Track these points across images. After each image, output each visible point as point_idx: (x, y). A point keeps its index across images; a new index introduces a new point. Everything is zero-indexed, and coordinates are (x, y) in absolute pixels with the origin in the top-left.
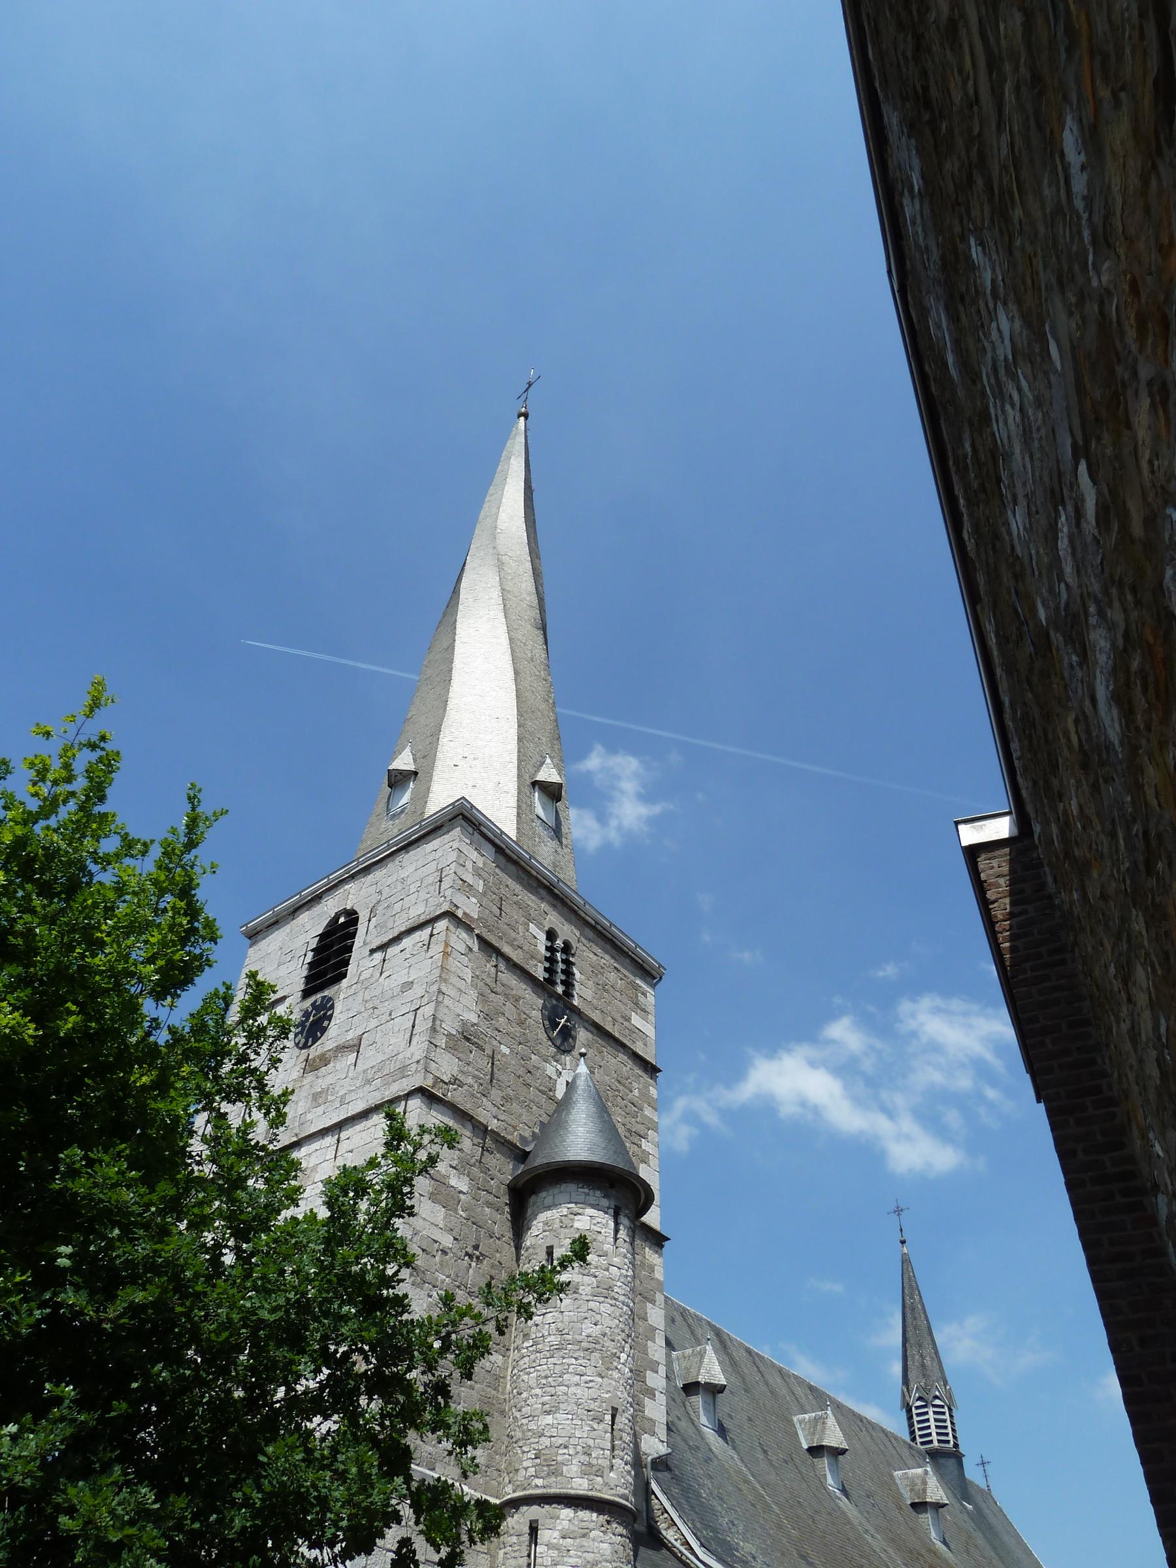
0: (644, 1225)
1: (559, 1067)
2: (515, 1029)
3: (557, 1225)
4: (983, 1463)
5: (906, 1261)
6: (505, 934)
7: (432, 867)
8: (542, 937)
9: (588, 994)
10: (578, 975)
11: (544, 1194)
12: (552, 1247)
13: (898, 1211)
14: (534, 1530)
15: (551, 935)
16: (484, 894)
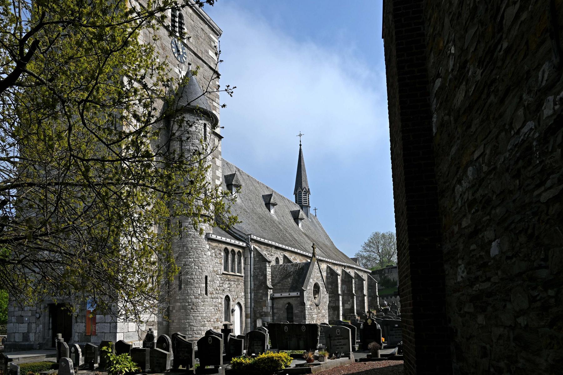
5: (300, 149)
10: (186, 30)
13: (300, 135)
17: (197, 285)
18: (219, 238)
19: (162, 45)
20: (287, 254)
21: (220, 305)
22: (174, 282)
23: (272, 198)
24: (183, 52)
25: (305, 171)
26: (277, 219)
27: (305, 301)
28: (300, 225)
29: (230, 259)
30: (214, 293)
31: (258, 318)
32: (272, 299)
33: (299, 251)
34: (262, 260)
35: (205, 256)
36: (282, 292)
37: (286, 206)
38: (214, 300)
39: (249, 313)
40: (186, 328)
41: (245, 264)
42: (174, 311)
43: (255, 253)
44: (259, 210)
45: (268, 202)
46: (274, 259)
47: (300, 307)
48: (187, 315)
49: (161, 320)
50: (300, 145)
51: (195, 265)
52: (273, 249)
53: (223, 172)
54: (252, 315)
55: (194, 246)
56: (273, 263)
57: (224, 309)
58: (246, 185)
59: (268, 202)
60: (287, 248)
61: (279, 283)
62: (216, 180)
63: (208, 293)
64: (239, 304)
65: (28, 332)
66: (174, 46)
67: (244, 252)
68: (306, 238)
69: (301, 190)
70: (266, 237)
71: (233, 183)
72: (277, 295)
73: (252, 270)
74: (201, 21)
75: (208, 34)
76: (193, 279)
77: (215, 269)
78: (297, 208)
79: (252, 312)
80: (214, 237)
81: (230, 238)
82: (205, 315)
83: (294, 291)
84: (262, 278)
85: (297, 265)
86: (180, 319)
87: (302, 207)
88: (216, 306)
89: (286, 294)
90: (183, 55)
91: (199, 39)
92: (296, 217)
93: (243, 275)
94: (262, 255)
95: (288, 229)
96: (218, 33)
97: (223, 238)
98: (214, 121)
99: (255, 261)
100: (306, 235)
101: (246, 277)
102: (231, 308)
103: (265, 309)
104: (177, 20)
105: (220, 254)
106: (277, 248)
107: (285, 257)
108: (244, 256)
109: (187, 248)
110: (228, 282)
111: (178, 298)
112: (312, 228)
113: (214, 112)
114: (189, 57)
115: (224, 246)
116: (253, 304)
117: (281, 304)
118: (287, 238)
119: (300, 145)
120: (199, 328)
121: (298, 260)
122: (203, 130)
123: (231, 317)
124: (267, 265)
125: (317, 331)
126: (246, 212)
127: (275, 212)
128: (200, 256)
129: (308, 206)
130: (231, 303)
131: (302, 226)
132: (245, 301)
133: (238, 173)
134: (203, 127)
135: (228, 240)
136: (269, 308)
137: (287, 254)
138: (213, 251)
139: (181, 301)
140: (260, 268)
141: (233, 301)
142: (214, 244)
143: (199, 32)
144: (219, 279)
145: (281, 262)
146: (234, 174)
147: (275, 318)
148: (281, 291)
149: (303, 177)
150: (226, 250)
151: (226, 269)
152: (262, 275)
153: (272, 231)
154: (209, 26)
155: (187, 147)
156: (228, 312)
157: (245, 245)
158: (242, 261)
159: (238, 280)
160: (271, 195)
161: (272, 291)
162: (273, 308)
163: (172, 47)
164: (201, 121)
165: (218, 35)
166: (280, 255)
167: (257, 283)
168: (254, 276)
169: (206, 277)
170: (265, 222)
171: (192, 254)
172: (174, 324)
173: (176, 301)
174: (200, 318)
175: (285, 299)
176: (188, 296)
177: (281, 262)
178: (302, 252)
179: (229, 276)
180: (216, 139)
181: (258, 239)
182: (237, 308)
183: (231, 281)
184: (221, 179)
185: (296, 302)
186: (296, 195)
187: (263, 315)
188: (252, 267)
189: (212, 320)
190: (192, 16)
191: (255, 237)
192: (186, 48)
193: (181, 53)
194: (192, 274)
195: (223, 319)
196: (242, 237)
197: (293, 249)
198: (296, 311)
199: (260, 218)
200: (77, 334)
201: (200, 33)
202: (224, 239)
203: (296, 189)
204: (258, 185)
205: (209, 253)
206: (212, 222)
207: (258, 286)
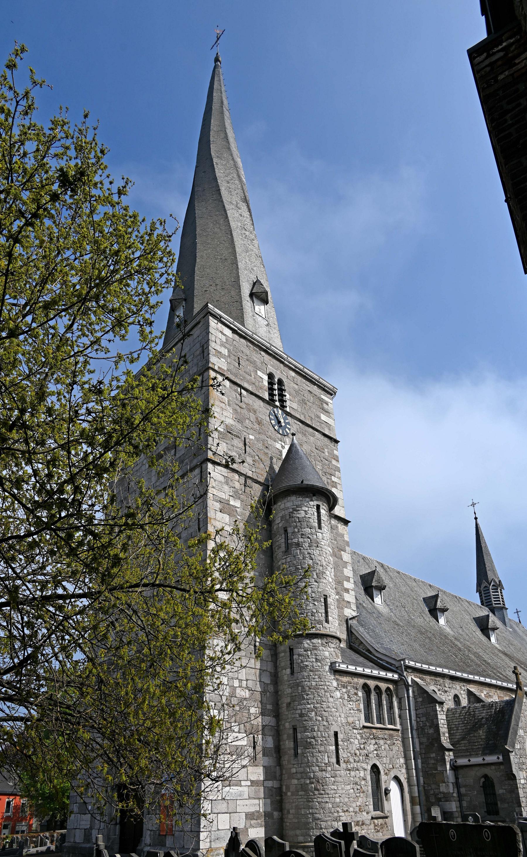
0: (333, 514)
1: (283, 444)
2: (256, 426)
3: (288, 517)
4: (517, 612)
5: (477, 525)
6: (244, 377)
7: (198, 345)
8: (266, 378)
9: (295, 406)
10: (288, 397)
11: (279, 504)
12: (286, 527)
13: (473, 505)
14: (291, 650)
15: (271, 376)
16: (229, 356)
17: (322, 749)
18: (351, 668)
19: (257, 419)
20: (473, 689)
21: (363, 782)
22: (288, 744)
23: (439, 600)
24: (285, 422)
25: (490, 555)
26: (452, 633)
27: (514, 771)
28: (493, 639)
29: (373, 701)
30: (352, 760)
31: (433, 804)
32: (455, 768)
33: (494, 682)
34: (427, 701)
35: (331, 700)
36: (470, 755)
37: (465, 610)
38: (353, 773)
39: (416, 794)
40: (309, 823)
41: (400, 708)
42: (289, 794)
43: (416, 689)
44: (419, 621)
45: (433, 607)
46: (451, 697)
47: (507, 782)
48: (309, 800)
49: (269, 809)
50: (476, 518)
51: (316, 715)
52: (447, 681)
53: (354, 570)
54: (423, 798)
55: (314, 684)
56: (450, 704)
57: (370, 788)
58: (395, 585)
59: (433, 607)
60: (471, 677)
61: (463, 739)
62: (345, 583)
63: (341, 762)
64: (397, 779)
65: (91, 828)
66: (273, 418)
67: (396, 690)
68: (507, 660)
69: (487, 585)
70: (433, 662)
71: (373, 584)
72: (462, 761)
73: (413, 718)
74: (308, 383)
75: (318, 395)
76: (314, 738)
77: (350, 720)
78: (484, 612)
79: (423, 793)
80: (343, 667)
81: (372, 668)
82: (338, 800)
83: (491, 753)
84: (431, 731)
85: (491, 705)
86: (298, 808)
87: (493, 610)
88: (356, 784)
89: (475, 760)
90: (285, 425)
91: (306, 404)
92: (483, 625)
93: (399, 727)
94: (426, 692)
95: (473, 646)
96: (331, 393)
97: (358, 668)
98: (332, 501)
99: (416, 702)
100: (506, 654)
101: (404, 731)
102: (383, 788)
103: (443, 788)
104: (276, 387)
105: (356, 694)
106: (453, 678)
107: (470, 694)
108: (397, 696)
109: (303, 687)
110: (373, 741)
111: (294, 770)
112: (515, 642)
113: (334, 490)
114: (294, 426)
115: (362, 681)
116: (421, 779)
117: (470, 778)
118: (472, 661)
119: (476, 518)
120: (329, 823)
121: (495, 697)
122: (316, 514)
123: (385, 802)
124: (438, 708)
125: (515, 842)
126: (398, 625)
127: (447, 622)
128: (324, 699)
129: (504, 608)
130: (383, 777)
131: (497, 640)
132: (408, 773)
133: (379, 569)
134: (315, 510)
135: (368, 671)
136: (451, 786)
137: (473, 689)
138: (344, 690)
139: (299, 776)
140: (426, 715)
141: (386, 774)
142: (345, 679)
143: (306, 395)
144: (358, 737)
145: (464, 702)
146: (374, 572)
147: (465, 804)
148: (469, 753)
149: (487, 565)
150: (366, 687)
151: (368, 718)
152: (430, 727)
153: (444, 652)
154: (319, 386)
155: (295, 540)
156: (379, 795)
157: (396, 677)
158: (395, 704)
159: (391, 736)
160: (437, 596)
161: (451, 753)
162: (457, 785)
163: (270, 419)
164: (312, 503)
165: (331, 395)
166: (460, 689)
167: (424, 740)
168: (417, 729)
169: (336, 734)
170: (430, 638)
171: (312, 697)
172: (291, 816)
173: (291, 776)
174: (330, 806)
175: (477, 768)
176: (309, 767)
177: (464, 702)
178: (499, 683)
179: (374, 731)
180: (339, 525)
181: (418, 665)
182: (394, 787)
183: (379, 739)
184: (352, 580)
185: (498, 774)
186: (480, 593)
187: (441, 799)
188: (413, 713)
189: (351, 809)
190: (295, 380)
191: (412, 664)
192: (289, 418)
193: (283, 424)
194: (313, 730)
195: (371, 807)
196: (391, 664)
197: (482, 679)
198: (500, 791)
199: (422, 633)
200: (149, 832)
201: (307, 395)
202: (360, 670)
203: (479, 584)
204: (414, 584)
205: (338, 694)
206: (343, 645)
207: (426, 746)
